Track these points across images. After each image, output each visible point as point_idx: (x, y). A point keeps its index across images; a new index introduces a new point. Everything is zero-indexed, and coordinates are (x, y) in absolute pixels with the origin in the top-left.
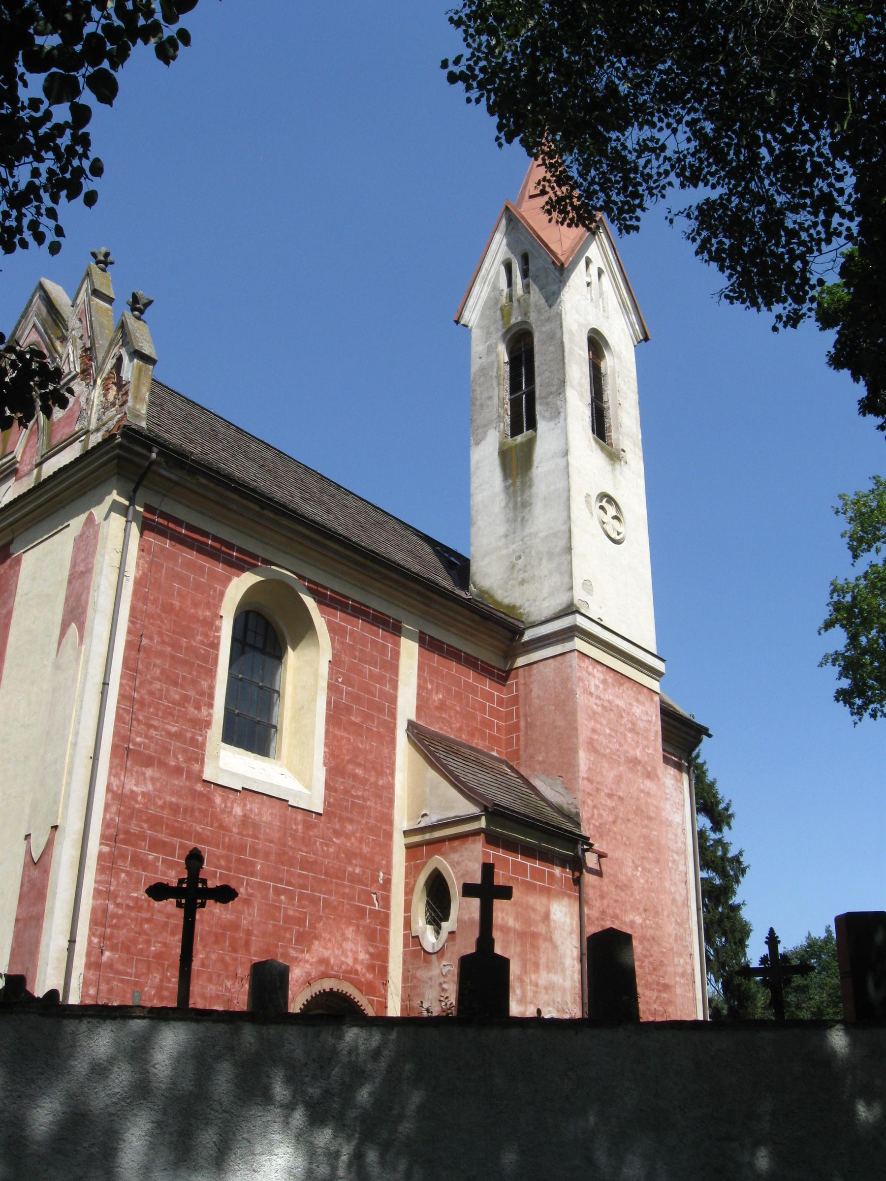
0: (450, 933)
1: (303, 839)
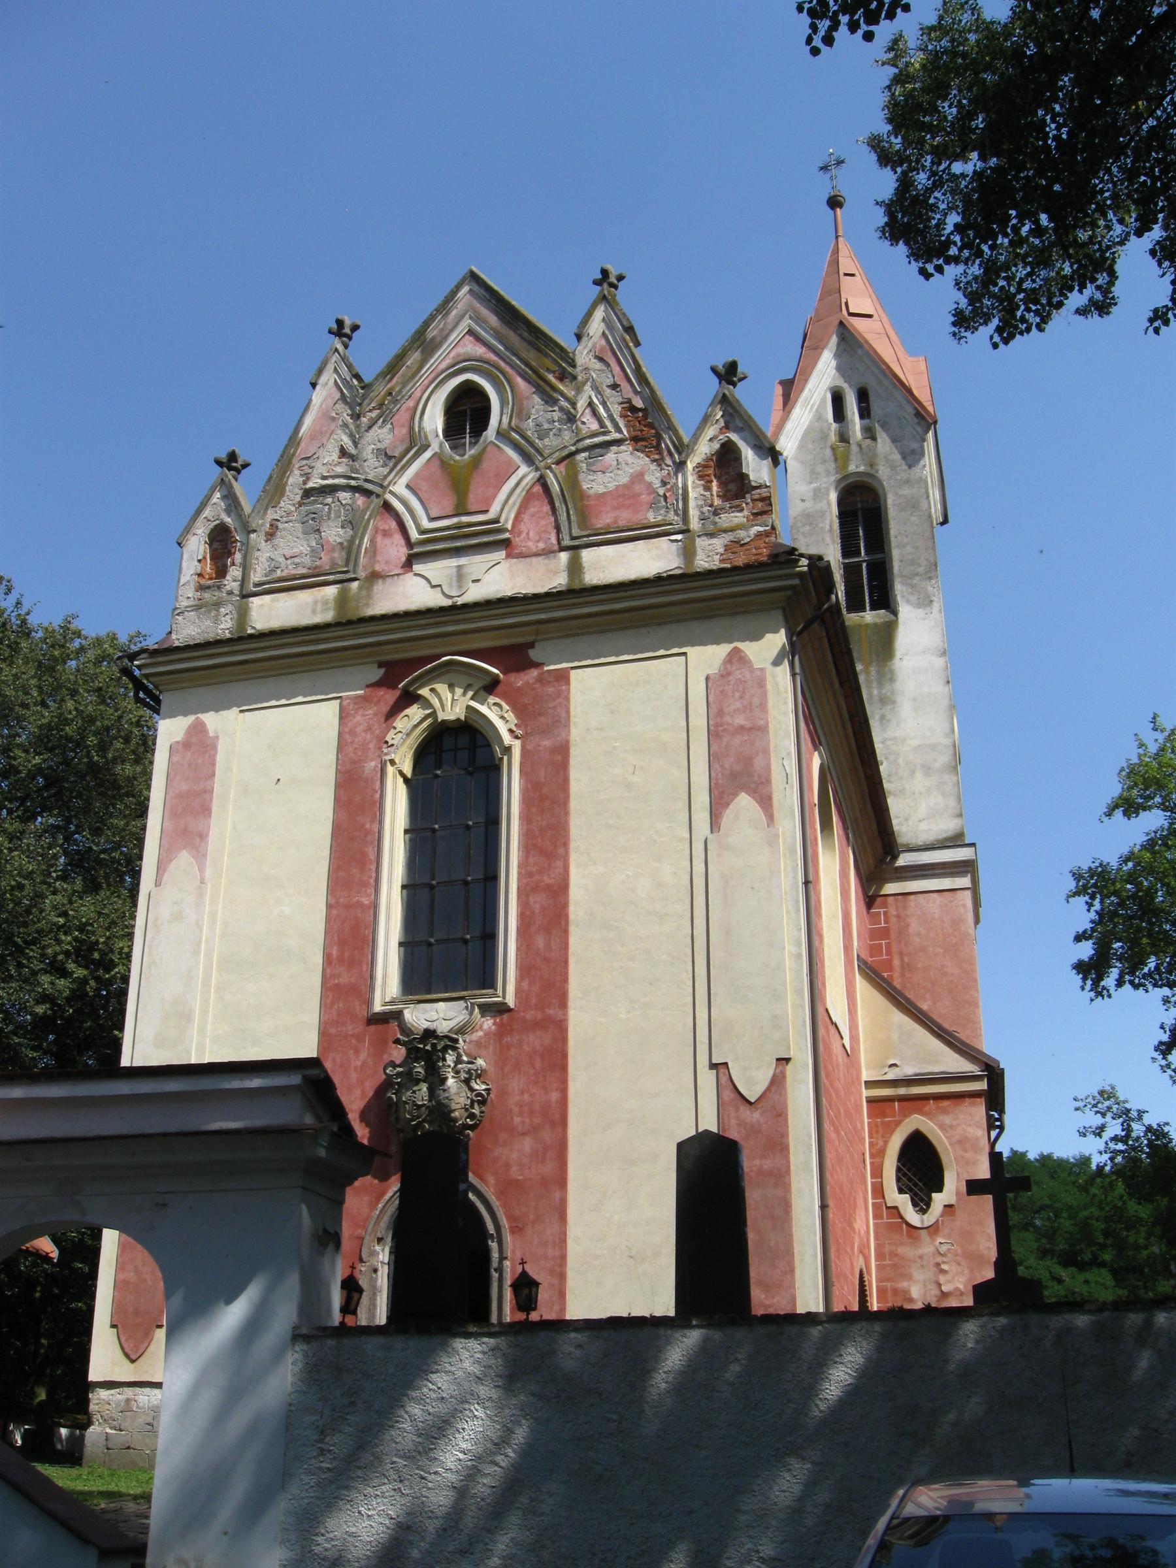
0: (945, 1206)
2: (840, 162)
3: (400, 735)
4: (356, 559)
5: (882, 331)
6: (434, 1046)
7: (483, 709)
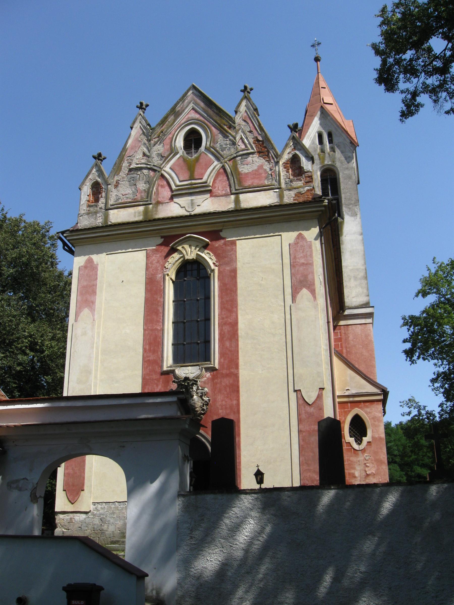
2: (319, 44)
3: (170, 264)
4: (151, 196)
5: (336, 110)
6: (188, 383)
7: (203, 255)
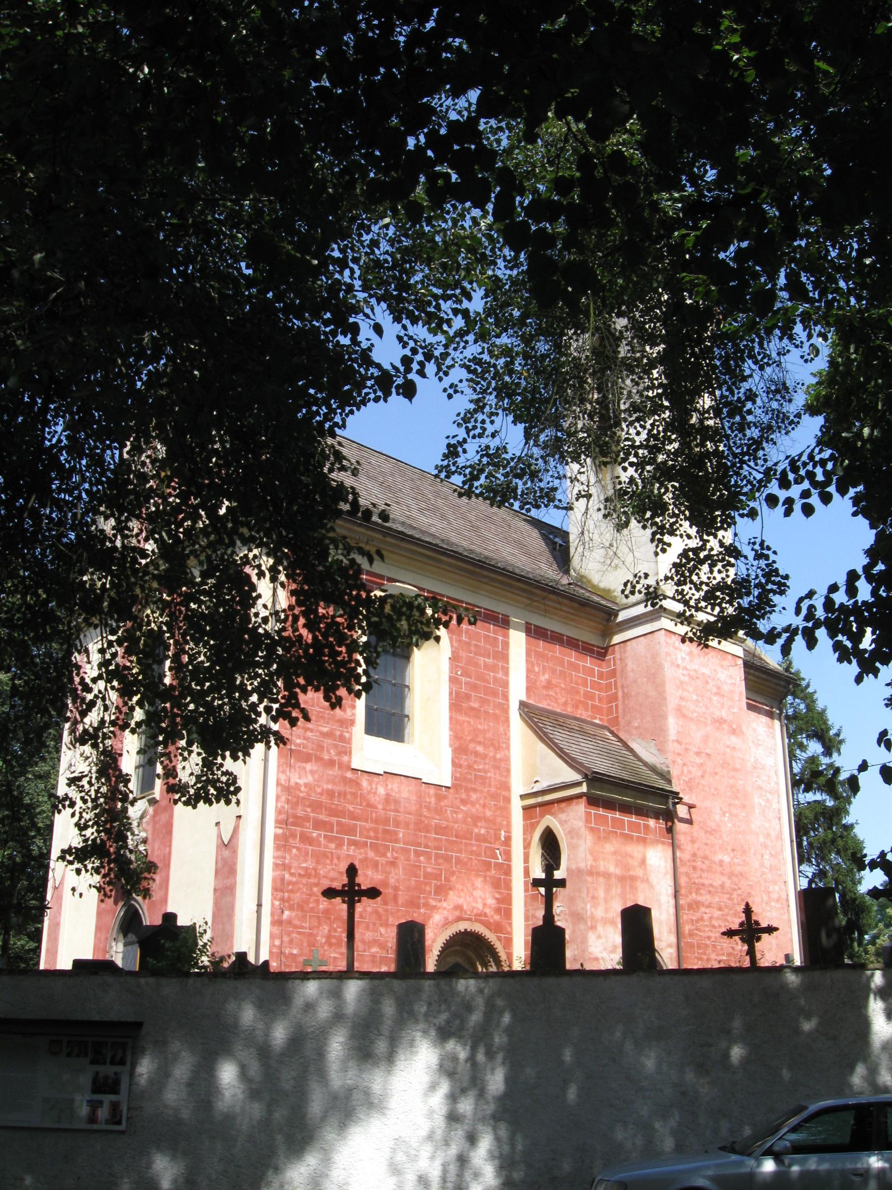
1: (436, 809)
